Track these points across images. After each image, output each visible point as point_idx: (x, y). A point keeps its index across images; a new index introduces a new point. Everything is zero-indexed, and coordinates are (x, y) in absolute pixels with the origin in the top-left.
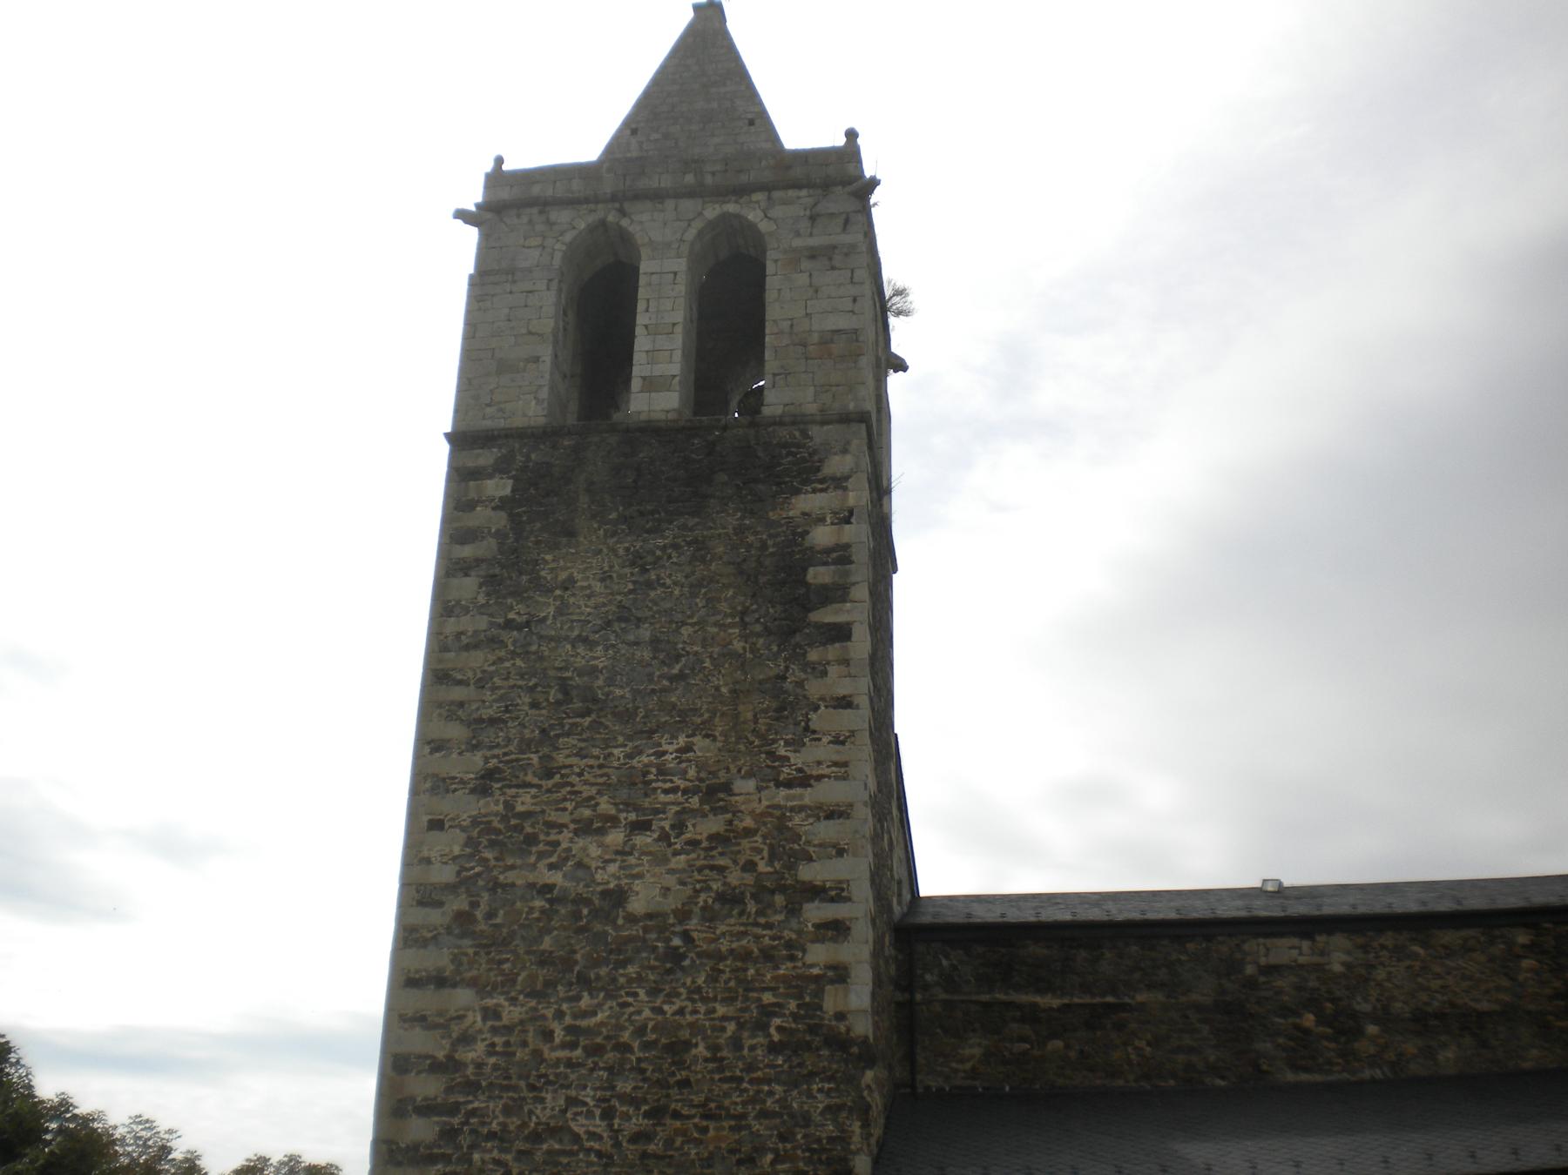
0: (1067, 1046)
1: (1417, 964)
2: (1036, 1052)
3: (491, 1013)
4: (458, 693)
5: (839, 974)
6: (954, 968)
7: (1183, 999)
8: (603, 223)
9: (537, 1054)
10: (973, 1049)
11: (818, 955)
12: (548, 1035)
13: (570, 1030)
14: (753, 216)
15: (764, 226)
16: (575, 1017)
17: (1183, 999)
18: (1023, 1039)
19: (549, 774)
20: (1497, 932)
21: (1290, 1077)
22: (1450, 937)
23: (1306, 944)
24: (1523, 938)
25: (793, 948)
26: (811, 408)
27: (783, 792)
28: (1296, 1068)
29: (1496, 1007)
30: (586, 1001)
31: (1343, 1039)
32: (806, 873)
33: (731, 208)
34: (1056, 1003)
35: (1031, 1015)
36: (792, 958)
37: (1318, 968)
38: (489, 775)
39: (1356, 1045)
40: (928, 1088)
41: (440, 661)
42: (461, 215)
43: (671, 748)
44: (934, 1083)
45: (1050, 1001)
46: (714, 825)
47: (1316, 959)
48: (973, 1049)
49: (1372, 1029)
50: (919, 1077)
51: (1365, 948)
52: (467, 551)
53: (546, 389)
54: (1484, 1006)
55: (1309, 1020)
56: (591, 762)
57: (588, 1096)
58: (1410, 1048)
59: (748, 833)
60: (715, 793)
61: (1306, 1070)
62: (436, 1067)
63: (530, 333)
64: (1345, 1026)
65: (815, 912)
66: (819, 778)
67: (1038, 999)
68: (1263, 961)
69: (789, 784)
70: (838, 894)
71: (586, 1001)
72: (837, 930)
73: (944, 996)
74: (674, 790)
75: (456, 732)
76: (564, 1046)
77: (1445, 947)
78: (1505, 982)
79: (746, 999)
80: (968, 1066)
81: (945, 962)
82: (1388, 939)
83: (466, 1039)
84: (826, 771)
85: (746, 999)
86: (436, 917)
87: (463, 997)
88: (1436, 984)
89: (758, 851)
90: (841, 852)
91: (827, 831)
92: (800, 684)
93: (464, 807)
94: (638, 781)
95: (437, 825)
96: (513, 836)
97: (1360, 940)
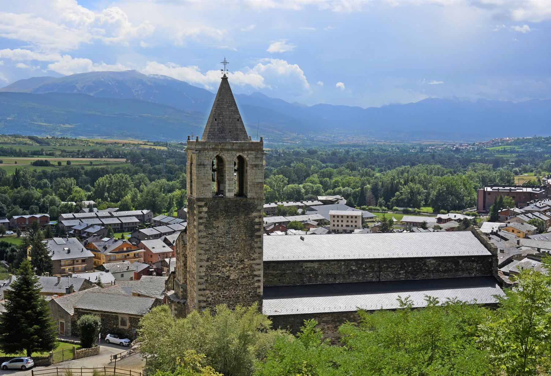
5: (259, 287)
32: (255, 273)
46: (242, 266)
52: (201, 221)
65: (256, 279)
70: (259, 276)
75: (202, 252)
87: (208, 292)
91: (257, 267)
93: (205, 264)
94: (230, 259)
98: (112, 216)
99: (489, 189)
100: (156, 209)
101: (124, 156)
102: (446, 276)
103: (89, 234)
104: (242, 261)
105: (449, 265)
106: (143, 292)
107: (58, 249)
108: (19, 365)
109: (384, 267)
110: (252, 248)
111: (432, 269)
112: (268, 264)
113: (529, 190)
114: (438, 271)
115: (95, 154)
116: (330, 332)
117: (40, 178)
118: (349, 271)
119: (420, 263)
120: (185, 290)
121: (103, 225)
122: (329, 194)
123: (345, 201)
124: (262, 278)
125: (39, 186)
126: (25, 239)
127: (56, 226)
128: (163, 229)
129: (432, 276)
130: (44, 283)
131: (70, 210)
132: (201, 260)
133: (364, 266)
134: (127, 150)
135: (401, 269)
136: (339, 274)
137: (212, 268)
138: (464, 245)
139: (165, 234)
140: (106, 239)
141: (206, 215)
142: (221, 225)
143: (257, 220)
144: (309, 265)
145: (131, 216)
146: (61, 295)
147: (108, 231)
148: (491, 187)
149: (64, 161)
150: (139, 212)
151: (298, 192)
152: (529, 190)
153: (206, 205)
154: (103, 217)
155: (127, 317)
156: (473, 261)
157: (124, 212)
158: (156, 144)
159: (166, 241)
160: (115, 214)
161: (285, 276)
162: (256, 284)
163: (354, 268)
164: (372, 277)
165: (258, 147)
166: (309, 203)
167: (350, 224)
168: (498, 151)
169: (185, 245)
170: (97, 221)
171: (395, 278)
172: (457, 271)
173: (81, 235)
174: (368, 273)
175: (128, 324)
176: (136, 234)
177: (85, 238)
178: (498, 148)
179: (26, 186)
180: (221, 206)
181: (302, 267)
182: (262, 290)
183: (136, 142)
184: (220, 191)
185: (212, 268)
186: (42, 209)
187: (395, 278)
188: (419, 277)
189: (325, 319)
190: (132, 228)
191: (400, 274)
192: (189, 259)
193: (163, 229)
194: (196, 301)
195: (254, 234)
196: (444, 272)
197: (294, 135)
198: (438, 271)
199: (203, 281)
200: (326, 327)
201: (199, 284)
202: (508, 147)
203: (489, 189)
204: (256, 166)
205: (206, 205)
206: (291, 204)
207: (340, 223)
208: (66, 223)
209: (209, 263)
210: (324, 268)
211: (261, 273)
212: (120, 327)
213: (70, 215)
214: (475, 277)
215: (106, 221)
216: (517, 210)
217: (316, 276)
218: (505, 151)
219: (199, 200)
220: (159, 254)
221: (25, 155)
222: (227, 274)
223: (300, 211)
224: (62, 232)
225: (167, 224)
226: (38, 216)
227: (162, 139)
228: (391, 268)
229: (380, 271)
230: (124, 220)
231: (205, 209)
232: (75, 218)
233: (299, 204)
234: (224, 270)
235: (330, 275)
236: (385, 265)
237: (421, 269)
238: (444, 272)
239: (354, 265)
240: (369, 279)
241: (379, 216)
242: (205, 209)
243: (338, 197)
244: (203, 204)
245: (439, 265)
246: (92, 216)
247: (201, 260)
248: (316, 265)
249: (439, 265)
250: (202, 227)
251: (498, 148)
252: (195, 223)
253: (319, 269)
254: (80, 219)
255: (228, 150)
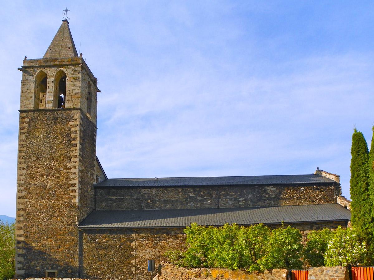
0: (116, 204)
1: (165, 193)
2: (112, 205)
3: (30, 202)
4: (23, 154)
5: (75, 197)
6: (102, 193)
7: (132, 198)
8: (42, 71)
9: (36, 208)
10: (104, 205)
11: (72, 194)
12: (38, 205)
13: (41, 205)
14: (65, 70)
15: (66, 72)
16: (41, 203)
17: (132, 198)
18: (111, 203)
19: (36, 167)
20: (177, 189)
21: (146, 209)
22: (170, 189)
23: (150, 190)
24: (180, 190)
25: (68, 193)
26: (72, 107)
27: (67, 170)
28: (147, 208)
29: (175, 200)
30: (42, 201)
31: (154, 204)
32: (70, 182)
33: (61, 69)
34: (115, 198)
35: (112, 200)
36: (68, 195)
37: (151, 193)
38: (28, 167)
39: (155, 205)
40: (98, 210)
41: (20, 149)
42: (19, 69)
43: (52, 163)
44: (99, 209)
45: (115, 198)
46: (58, 175)
47: (151, 192)
48: (104, 205)
49: (158, 203)
50: (97, 208)
51: (158, 191)
52: (23, 131)
53: (33, 103)
54: (174, 200)
55: (149, 201)
56: (41, 165)
57: (43, 214)
58: (163, 205)
59: (62, 176)
60: (58, 171)
61: (148, 208)
62: (23, 210)
63: (31, 92)
64: (154, 202)
65: (71, 188)
66: (72, 168)
67: (113, 198)
68: (144, 192)
69: (68, 169)
70: (74, 185)
71: (42, 201)
72: (74, 191)
73: (100, 197)
74: (53, 170)
75: (23, 160)
76: (39, 207)
77: (169, 191)
78: (177, 196)
79: (63, 200)
80: (103, 207)
81: (101, 192)
82: (161, 189)
83: (27, 206)
84: (73, 167)
85: (63, 200)
86: (22, 189)
87: (26, 200)
88: (167, 196)
89: (64, 179)
90: (75, 179)
91: (72, 176)
92: (70, 154)
93: (24, 172)
94: (48, 168)
95: (21, 175)
96: (32, 176)
97: (157, 190)
109: (223, 195)
111: (273, 196)
116: (148, 249)
118: (186, 198)
119: (260, 191)
133: (202, 193)
136: (177, 201)
137: (32, 176)
157: (165, 225)
161: (123, 201)
163: (191, 195)
164: (211, 204)
171: (234, 205)
174: (206, 200)
181: (140, 193)
182: (77, 200)
187: (234, 205)
191: (239, 201)
200: (144, 243)
211: (76, 182)
228: (230, 195)
229: (218, 199)
235: (167, 201)
236: (223, 192)
237: (262, 197)
239: (191, 192)
240: (207, 206)
253: (156, 195)
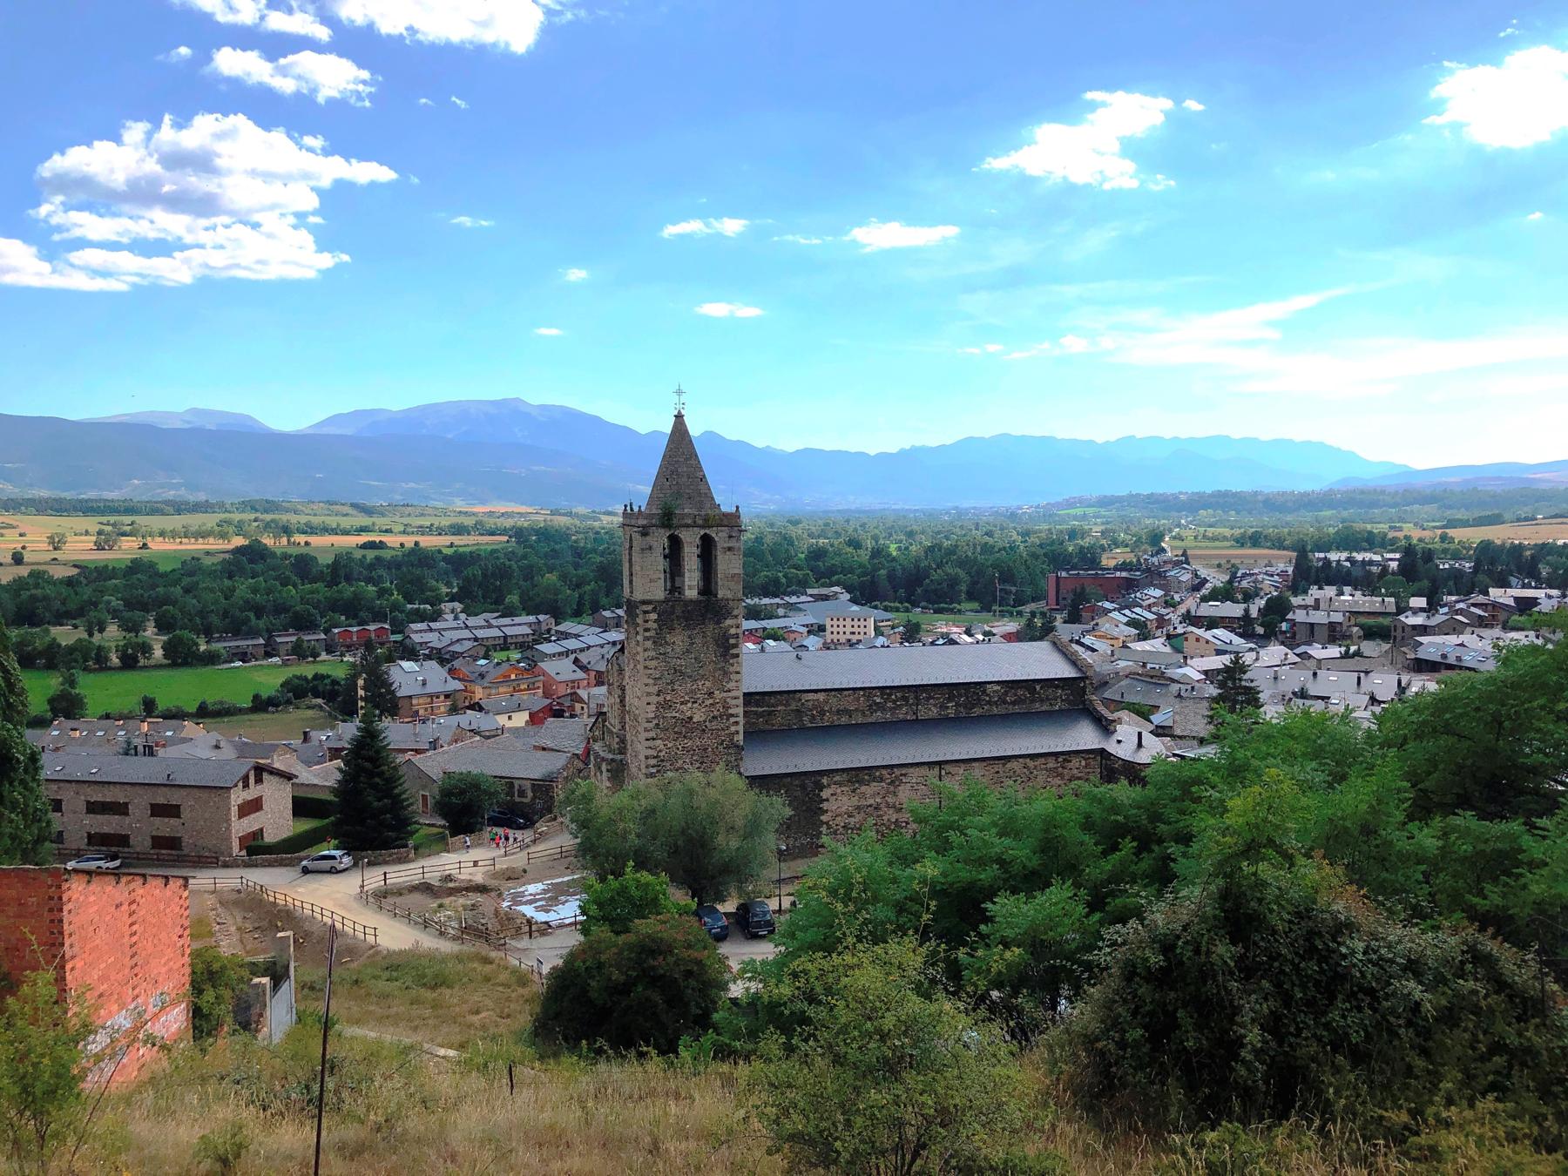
65: (732, 720)
91: (734, 702)
93: (654, 699)
94: (692, 691)
98: (490, 626)
99: (1064, 574)
100: (558, 617)
101: (504, 532)
102: (1017, 709)
103: (455, 656)
104: (711, 694)
105: (1020, 692)
106: (549, 744)
107: (407, 676)
108: (326, 864)
110: (726, 673)
112: (748, 696)
113: (1124, 574)
114: (1005, 702)
115: (458, 530)
117: (371, 567)
120: (623, 741)
121: (476, 639)
122: (823, 586)
123: (848, 596)
124: (741, 719)
125: (369, 580)
126: (353, 665)
127: (401, 643)
128: (572, 644)
129: (995, 710)
130: (395, 732)
131: (421, 617)
132: (649, 694)
134: (509, 523)
135: (949, 700)
138: (1039, 662)
139: (574, 651)
140: (482, 662)
141: (655, 626)
142: (678, 640)
143: (733, 631)
144: (811, 696)
145: (520, 626)
146: (417, 751)
147: (487, 649)
148: (1067, 570)
149: (409, 541)
150: (532, 618)
151: (776, 581)
152: (1124, 574)
153: (654, 610)
154: (476, 628)
155: (528, 784)
156: (1057, 687)
158: (554, 513)
159: (576, 661)
160: (494, 622)
162: (733, 729)
165: (731, 521)
166: (794, 599)
167: (856, 630)
168: (1075, 518)
169: (621, 671)
170: (466, 634)
172: (1032, 701)
173: (442, 657)
175: (530, 794)
176: (529, 653)
177: (448, 661)
178: (1072, 512)
179: (348, 579)
180: (678, 611)
182: (741, 737)
183: (523, 509)
184: (675, 589)
185: (666, 705)
186: (379, 616)
188: (977, 711)
189: (837, 778)
190: (524, 646)
192: (628, 692)
193: (572, 644)
194: (642, 757)
195: (727, 648)
196: (1014, 703)
197: (767, 496)
198: (1005, 702)
199: (651, 725)
201: (646, 730)
202: (1090, 511)
203: (1064, 574)
204: (730, 549)
205: (654, 610)
206: (766, 601)
207: (841, 630)
208: (416, 638)
209: (661, 699)
210: (833, 701)
211: (740, 711)
212: (517, 799)
213: (420, 626)
214: (1061, 711)
215: (480, 634)
216: (1107, 605)
217: (822, 713)
218: (1084, 517)
219: (644, 602)
220: (566, 683)
221: (346, 533)
222: (689, 714)
223: (781, 612)
224: (411, 653)
225: (577, 636)
226: (372, 627)
227: (563, 504)
230: (509, 631)
231: (654, 616)
232: (431, 630)
233: (777, 600)
234: (684, 708)
238: (1014, 703)
241: (900, 617)
242: (654, 616)
243: (836, 589)
244: (650, 608)
245: (1006, 693)
246: (453, 627)
247: (649, 694)
248: (848, 703)
249: (1006, 693)
250: (649, 644)
251: (1072, 512)
252: (639, 638)
254: (439, 631)
255: (688, 526)
